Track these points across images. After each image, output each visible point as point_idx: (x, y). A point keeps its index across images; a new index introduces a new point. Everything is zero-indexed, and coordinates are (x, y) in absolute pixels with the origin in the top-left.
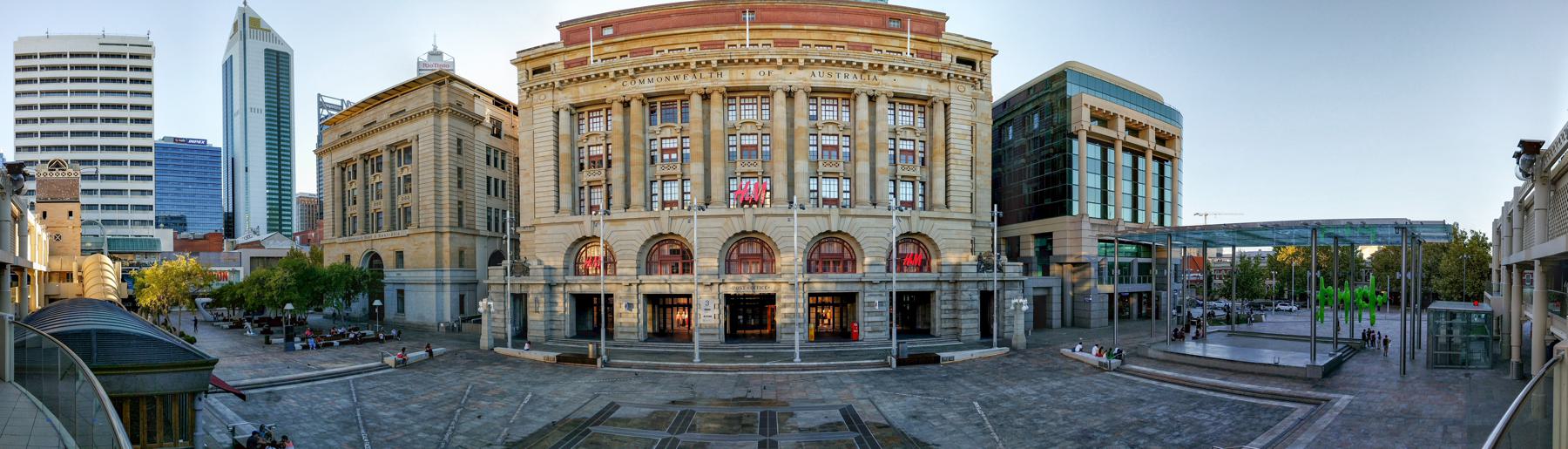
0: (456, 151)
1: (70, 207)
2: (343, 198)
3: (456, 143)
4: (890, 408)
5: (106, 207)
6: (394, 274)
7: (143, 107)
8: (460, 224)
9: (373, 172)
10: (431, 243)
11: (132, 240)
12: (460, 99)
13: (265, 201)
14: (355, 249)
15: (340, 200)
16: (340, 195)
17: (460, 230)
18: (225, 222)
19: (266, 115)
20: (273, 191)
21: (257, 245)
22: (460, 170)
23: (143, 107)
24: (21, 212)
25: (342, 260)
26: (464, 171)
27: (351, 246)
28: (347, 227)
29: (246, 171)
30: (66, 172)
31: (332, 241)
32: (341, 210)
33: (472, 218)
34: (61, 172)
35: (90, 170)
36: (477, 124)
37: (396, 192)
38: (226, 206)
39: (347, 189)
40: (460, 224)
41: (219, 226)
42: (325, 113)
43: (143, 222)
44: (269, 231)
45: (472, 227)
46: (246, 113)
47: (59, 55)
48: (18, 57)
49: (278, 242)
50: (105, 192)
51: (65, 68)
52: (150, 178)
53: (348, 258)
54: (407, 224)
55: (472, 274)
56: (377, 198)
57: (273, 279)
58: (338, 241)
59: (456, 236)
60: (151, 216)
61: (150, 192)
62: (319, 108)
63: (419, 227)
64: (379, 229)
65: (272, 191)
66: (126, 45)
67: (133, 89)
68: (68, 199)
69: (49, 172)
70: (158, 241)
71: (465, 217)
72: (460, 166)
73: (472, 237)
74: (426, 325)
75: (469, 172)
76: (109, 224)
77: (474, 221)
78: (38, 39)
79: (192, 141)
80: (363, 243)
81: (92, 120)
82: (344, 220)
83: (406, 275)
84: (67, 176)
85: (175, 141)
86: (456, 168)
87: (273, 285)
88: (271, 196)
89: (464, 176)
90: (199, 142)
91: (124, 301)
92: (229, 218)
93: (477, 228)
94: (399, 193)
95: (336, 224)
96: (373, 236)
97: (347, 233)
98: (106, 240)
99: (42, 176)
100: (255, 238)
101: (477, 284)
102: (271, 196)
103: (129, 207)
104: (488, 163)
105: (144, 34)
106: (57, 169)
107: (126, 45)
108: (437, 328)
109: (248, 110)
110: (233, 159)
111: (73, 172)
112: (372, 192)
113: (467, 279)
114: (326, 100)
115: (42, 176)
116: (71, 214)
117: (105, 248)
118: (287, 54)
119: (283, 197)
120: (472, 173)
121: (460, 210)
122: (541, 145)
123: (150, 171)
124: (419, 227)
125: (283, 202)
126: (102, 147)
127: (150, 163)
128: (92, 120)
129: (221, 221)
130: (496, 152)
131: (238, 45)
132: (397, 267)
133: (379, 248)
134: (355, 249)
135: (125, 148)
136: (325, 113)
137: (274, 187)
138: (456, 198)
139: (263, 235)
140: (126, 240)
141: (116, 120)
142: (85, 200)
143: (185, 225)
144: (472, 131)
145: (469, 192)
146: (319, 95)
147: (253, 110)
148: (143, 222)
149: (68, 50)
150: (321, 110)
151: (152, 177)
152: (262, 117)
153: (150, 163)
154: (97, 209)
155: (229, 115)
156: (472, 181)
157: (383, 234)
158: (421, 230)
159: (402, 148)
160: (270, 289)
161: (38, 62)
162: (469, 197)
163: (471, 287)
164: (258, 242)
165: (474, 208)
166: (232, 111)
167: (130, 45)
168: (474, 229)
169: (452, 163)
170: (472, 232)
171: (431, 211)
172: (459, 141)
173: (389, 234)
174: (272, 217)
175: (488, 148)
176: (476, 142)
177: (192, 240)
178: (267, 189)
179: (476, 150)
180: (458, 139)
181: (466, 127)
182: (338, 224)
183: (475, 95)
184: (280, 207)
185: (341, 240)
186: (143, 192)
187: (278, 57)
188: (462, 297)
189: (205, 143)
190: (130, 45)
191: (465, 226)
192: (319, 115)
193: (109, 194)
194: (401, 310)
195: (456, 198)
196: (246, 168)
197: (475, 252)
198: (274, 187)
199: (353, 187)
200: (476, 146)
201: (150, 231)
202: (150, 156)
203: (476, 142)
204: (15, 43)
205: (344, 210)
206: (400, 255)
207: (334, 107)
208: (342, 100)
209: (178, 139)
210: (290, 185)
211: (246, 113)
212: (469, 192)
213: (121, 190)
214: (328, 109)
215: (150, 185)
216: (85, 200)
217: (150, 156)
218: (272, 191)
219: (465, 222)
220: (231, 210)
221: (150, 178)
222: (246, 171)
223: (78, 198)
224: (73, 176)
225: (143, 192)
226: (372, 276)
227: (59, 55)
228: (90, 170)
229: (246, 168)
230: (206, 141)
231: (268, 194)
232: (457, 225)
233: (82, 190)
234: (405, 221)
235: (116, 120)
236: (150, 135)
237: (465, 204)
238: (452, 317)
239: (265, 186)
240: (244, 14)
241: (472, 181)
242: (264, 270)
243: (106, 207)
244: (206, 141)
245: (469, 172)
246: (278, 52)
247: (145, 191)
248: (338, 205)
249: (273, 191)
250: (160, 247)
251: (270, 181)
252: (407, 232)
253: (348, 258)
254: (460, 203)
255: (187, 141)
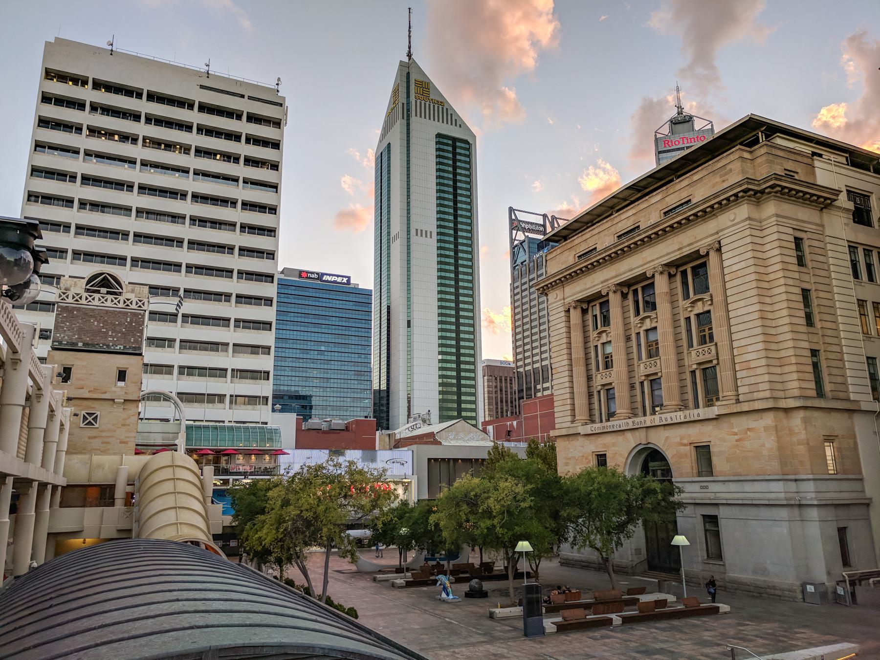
0: (795, 260)
1: (122, 361)
2: (587, 359)
3: (793, 246)
4: (448, 595)
5: (188, 370)
6: (696, 487)
7: (261, 208)
8: (820, 393)
9: (638, 313)
10: (766, 429)
11: (231, 429)
12: (790, 165)
13: (437, 373)
14: (614, 445)
15: (582, 362)
16: (581, 354)
17: (822, 403)
18: (375, 404)
19: (439, 241)
20: (449, 357)
21: (430, 439)
22: (805, 294)
23: (261, 208)
24: (15, 352)
25: (593, 463)
26: (813, 295)
27: (608, 439)
28: (596, 406)
29: (409, 326)
30: (121, 298)
31: (571, 431)
32: (584, 380)
33: (840, 380)
34: (110, 297)
35: (166, 304)
36: (827, 206)
37: (635, 355)
38: (377, 382)
39: (591, 345)
40: (820, 393)
41: (363, 410)
42: (520, 236)
43: (253, 400)
44: (443, 418)
45: (842, 395)
46: (409, 239)
47: (129, 92)
48: (49, 74)
49: (462, 435)
50: (188, 344)
51: (136, 117)
52: (266, 326)
53: (602, 459)
54: (712, 395)
55: (856, 485)
56: (650, 356)
57: (493, 495)
58: (582, 430)
59: (817, 414)
60: (265, 388)
61: (266, 349)
62: (511, 229)
63: (738, 401)
64: (611, 415)
65: (445, 357)
66: (243, 96)
67: (253, 111)
68: (119, 348)
69: (85, 295)
70: (276, 431)
71: (826, 379)
72: (806, 286)
73: (846, 415)
74: (774, 588)
75: (822, 295)
76: (190, 401)
77: (845, 384)
78: (95, 51)
79: (329, 278)
80: (629, 435)
81: (175, 218)
82: (590, 395)
83: (717, 490)
84: (121, 305)
85: (300, 276)
86: (798, 291)
87: (496, 508)
88: (445, 365)
89: (815, 302)
90: (339, 280)
91: (216, 537)
92: (381, 398)
93: (852, 397)
94: (691, 345)
95: (577, 402)
96: (649, 420)
97: (597, 418)
98: (183, 428)
99: (70, 300)
100: (425, 430)
101: (868, 505)
102: (445, 365)
103: (229, 372)
104: (856, 275)
105: (272, 85)
106: (104, 290)
107: (243, 96)
108: (800, 596)
109: (413, 232)
110: (389, 308)
111: (134, 300)
112: (639, 345)
113: (845, 497)
114: (521, 217)
115: (70, 300)
116: (122, 375)
117: (181, 442)
118: (467, 142)
119: (463, 366)
120: (828, 296)
121: (816, 366)
122: (741, 327)
123: (268, 314)
124: (738, 401)
125: (463, 382)
126: (189, 267)
127: (268, 301)
128: (175, 218)
129: (369, 403)
130: (868, 252)
131: (399, 127)
132: (700, 474)
133: (660, 440)
134: (614, 445)
135: (229, 272)
136: (520, 236)
137: (448, 350)
138: (805, 345)
139: (436, 427)
140: (218, 428)
141: (216, 224)
142: (152, 355)
143: (311, 408)
144: (818, 221)
145: (829, 332)
146: (511, 210)
147: (420, 233)
148: (253, 400)
149: (146, 87)
150: (514, 232)
151: (270, 324)
152: (432, 243)
153: (268, 301)
154: (171, 373)
155: (384, 240)
156: (831, 311)
157: (668, 415)
158: (745, 407)
159: (639, 287)
160: (488, 514)
161: (88, 94)
162: (828, 340)
163: (856, 512)
164: (432, 435)
165: (842, 360)
166: (389, 233)
167: (250, 98)
168: (848, 400)
169: (791, 282)
170: (846, 406)
171: (759, 371)
172: (798, 241)
173: (680, 416)
174: (446, 397)
175: (853, 248)
176: (828, 239)
177: (325, 432)
178: (440, 353)
179: (830, 254)
180: (796, 238)
181: (805, 214)
182: (581, 401)
183: (814, 154)
184: (459, 389)
185: (588, 429)
186: (255, 349)
187: (454, 147)
188: (842, 531)
189: (348, 282)
190: (250, 98)
191: (829, 395)
192: (512, 240)
193: (195, 349)
194: (716, 553)
195: (805, 345)
196: (409, 323)
197: (856, 443)
198: (448, 350)
199: (604, 338)
200: (829, 247)
201: (263, 414)
202: (270, 290)
203: (828, 239)
204: (48, 44)
205: (589, 378)
206: (704, 452)
207: (532, 228)
208: (545, 216)
209: (307, 272)
210: (473, 348)
211: (409, 239)
212: (829, 332)
213: (217, 344)
214: (524, 230)
215: (268, 338)
216: (152, 355)
217: (270, 290)
218: (445, 357)
219: (828, 387)
220: (384, 387)
221: (266, 326)
222: (409, 326)
223: (140, 348)
224: (134, 306)
225: (255, 349)
226: (662, 491)
227: (129, 92)
228: (166, 304)
229: (409, 323)
230: (349, 278)
231: (440, 361)
232: (813, 393)
233: (149, 339)
234: (707, 392)
235: (216, 224)
236: (271, 255)
237: (823, 356)
238: (829, 573)
239: (437, 349)
240: (408, 74)
241: (831, 311)
242: (476, 481)
243: (188, 370)
244: (349, 278)
245: (822, 295)
246: (455, 140)
247: (258, 347)
248: (579, 371)
249: (449, 357)
250: (280, 441)
251: (444, 342)
252: (715, 411)
253: (602, 459)
254: (814, 353)
255: (320, 276)
